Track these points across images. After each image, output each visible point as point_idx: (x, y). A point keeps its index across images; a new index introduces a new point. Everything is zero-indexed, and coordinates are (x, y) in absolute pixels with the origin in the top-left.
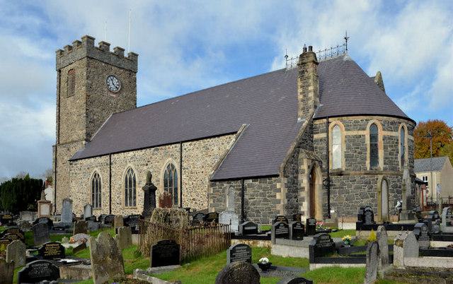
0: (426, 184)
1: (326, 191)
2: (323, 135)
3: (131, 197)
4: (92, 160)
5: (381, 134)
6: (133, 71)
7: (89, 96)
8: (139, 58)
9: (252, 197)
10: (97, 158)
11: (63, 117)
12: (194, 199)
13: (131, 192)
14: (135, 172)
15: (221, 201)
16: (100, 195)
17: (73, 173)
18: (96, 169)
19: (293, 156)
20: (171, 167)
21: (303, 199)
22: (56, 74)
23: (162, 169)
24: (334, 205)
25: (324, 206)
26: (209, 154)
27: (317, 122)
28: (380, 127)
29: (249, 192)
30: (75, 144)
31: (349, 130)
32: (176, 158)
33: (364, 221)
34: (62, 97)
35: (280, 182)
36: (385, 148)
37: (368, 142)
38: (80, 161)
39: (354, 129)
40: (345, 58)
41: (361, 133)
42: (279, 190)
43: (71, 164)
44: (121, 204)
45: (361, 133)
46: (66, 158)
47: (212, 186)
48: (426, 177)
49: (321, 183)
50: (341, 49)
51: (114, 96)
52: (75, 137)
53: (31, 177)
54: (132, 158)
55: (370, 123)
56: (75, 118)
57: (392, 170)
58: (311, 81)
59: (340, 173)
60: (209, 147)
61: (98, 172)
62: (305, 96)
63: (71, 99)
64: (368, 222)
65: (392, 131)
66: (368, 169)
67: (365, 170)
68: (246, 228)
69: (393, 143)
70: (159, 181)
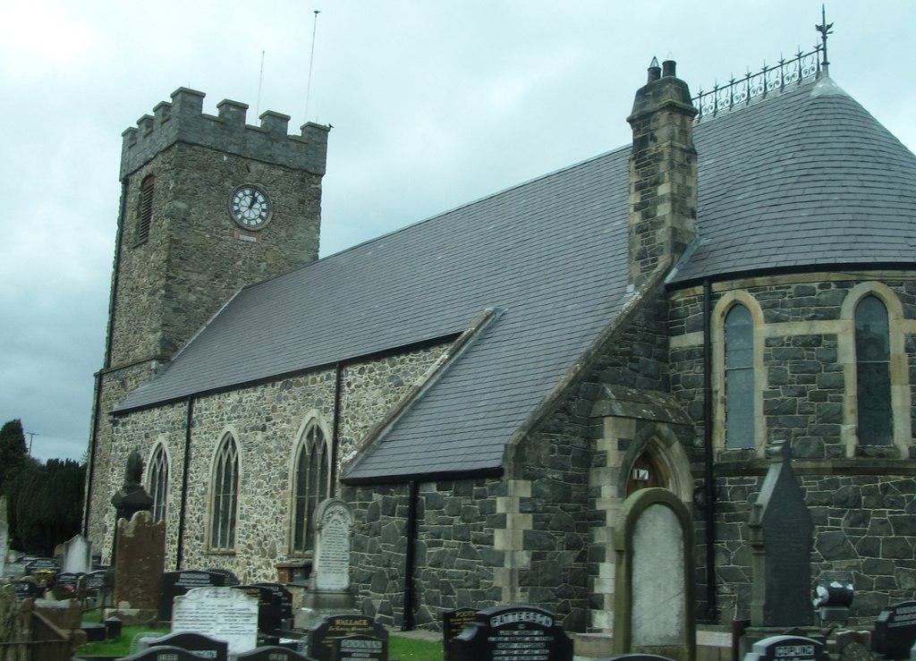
2: (695, 339)
4: (156, 412)
6: (313, 172)
7: (176, 242)
11: (124, 300)
18: (161, 439)
19: (565, 410)
20: (314, 433)
21: (599, 555)
23: (296, 441)
27: (679, 297)
28: (895, 306)
29: (429, 520)
30: (136, 370)
31: (777, 320)
34: (124, 248)
40: (820, 88)
41: (822, 327)
45: (822, 327)
50: (808, 63)
52: (139, 352)
55: (856, 293)
58: (663, 167)
60: (404, 379)
62: (646, 216)
63: (141, 251)
66: (850, 453)
70: (286, 476)
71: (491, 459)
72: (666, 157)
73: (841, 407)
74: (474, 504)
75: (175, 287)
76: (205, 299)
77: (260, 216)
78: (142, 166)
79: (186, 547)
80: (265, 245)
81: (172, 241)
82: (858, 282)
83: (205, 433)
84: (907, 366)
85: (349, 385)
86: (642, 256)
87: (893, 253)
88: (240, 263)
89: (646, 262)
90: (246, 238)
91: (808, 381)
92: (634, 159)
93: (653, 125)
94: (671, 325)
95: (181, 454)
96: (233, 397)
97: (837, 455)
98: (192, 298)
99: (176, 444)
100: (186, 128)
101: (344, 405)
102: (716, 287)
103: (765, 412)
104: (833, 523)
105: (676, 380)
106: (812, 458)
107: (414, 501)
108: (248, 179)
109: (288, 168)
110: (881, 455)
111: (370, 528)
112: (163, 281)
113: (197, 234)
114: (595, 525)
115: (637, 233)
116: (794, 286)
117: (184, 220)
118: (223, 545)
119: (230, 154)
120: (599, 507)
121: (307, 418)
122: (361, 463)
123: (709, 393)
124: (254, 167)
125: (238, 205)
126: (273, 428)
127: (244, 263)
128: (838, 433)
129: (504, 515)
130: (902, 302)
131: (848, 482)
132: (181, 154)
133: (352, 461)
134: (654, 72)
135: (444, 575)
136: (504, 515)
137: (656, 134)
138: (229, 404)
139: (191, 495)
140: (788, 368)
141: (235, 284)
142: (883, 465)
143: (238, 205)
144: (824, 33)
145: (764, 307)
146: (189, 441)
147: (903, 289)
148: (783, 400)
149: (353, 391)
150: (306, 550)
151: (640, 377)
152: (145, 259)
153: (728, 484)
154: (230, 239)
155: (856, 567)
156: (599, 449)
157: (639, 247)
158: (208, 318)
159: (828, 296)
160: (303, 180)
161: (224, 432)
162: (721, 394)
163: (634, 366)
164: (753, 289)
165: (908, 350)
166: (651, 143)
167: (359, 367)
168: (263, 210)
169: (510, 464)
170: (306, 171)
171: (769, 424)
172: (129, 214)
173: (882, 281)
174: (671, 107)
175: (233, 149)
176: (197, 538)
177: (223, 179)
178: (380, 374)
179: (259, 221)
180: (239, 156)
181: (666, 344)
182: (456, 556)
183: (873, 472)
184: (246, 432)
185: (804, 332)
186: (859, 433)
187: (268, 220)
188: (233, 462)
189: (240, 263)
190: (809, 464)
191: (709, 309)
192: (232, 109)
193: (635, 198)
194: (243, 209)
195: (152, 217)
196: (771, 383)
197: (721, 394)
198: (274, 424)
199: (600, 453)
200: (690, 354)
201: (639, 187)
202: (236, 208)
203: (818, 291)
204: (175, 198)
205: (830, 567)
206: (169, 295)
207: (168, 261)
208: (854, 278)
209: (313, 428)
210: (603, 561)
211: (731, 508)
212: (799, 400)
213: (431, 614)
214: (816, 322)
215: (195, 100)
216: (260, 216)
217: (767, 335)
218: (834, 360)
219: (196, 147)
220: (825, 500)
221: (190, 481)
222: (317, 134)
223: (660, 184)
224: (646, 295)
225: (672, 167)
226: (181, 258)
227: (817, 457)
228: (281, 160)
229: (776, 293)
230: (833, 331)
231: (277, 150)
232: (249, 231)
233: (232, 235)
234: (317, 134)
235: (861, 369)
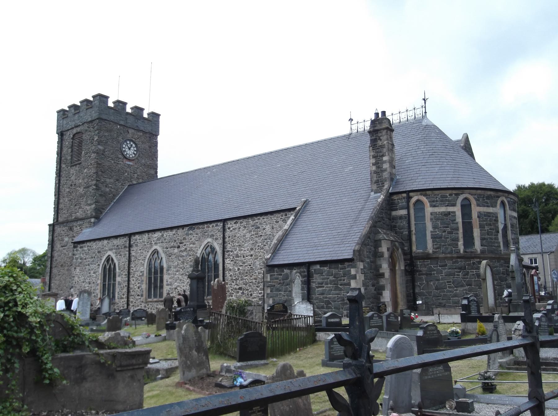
0: (537, 268)
1: (409, 278)
2: (404, 212)
3: (155, 287)
4: (105, 242)
5: (476, 210)
7: (100, 164)
8: (161, 119)
9: (320, 285)
10: (112, 240)
11: (65, 190)
12: (240, 289)
13: (156, 279)
14: (163, 255)
15: (280, 291)
16: (114, 285)
17: (77, 259)
18: (109, 253)
21: (383, 288)
22: (56, 138)
24: (421, 294)
25: (408, 296)
26: (260, 233)
27: (395, 197)
28: (474, 202)
31: (435, 206)
32: (216, 239)
33: (470, 312)
35: (355, 267)
36: (481, 227)
37: (459, 219)
38: (88, 244)
39: (441, 205)
40: (424, 123)
41: (450, 209)
42: (354, 277)
43: (75, 247)
44: (142, 296)
45: (450, 209)
46: (66, 239)
47: (268, 272)
48: (535, 260)
49: (403, 268)
51: (131, 163)
53: (546, 183)
54: (158, 239)
56: (81, 190)
57: (492, 252)
59: (427, 257)
61: (113, 256)
62: (378, 167)
64: (474, 314)
65: (488, 206)
66: (462, 251)
67: (458, 252)
68: (330, 320)
69: (491, 220)
71: (348, 255)
72: (386, 147)
73: (458, 236)
74: (340, 271)
75: (100, 185)
76: (113, 190)
77: (134, 153)
78: (73, 128)
79: (131, 300)
80: (136, 166)
81: (98, 164)
82: (462, 194)
83: (140, 250)
84: (478, 222)
85: (229, 228)
86: (377, 182)
87: (471, 184)
88: (126, 174)
89: (379, 184)
90: (129, 163)
91: (446, 227)
92: (371, 146)
93: (380, 135)
94: (392, 207)
95: (125, 260)
96: (158, 234)
97: (457, 252)
98: (108, 190)
99: (120, 255)
100: (102, 112)
101: (227, 236)
102: (411, 194)
103: (431, 238)
104: (457, 275)
105: (395, 226)
106: (449, 253)
107: (309, 271)
108: (128, 136)
109: (144, 132)
110: (472, 252)
111: (284, 283)
112: (94, 182)
113: (109, 161)
114: (379, 278)
115: (374, 173)
116: (440, 195)
117: (103, 154)
118: (155, 296)
119: (121, 125)
120: (381, 271)
121: (205, 242)
122: (272, 259)
123: (410, 232)
124: (131, 131)
125: (124, 148)
126: (185, 247)
127: (128, 174)
128: (457, 245)
129: (356, 275)
130: (476, 201)
131: (461, 261)
132: (99, 124)
133: (270, 258)
134: (377, 114)
135: (326, 298)
136: (356, 275)
137: (381, 138)
138: (155, 237)
139: (132, 277)
140: (439, 223)
141: (125, 183)
142: (473, 256)
143: (124, 148)
144: (425, 101)
145: (429, 202)
146: (130, 254)
147: (476, 196)
148: (438, 234)
149: (232, 231)
150: (207, 296)
151: (385, 226)
152: (80, 171)
153: (418, 263)
154: (122, 163)
155: (465, 290)
156: (380, 251)
157: (375, 179)
158: (114, 199)
159: (452, 198)
160: (150, 137)
161: (153, 249)
162: (414, 232)
163: (384, 222)
164: (425, 195)
165: (478, 217)
166: (379, 141)
167: (235, 221)
168: (135, 151)
169: (357, 257)
170: (152, 133)
171: (433, 242)
172: (65, 150)
173: (469, 194)
174: (387, 128)
175: (122, 123)
176: (138, 295)
177: (118, 136)
178: (247, 224)
179: (133, 155)
180: (125, 126)
181: (390, 214)
182: (332, 290)
183: (469, 258)
184: (167, 249)
185: (444, 211)
186: (465, 245)
187: (137, 155)
188: (112, 267)
189: (126, 174)
190: (449, 255)
191: (408, 202)
192: (121, 104)
193: (373, 161)
194: (127, 150)
195: (83, 152)
196: (433, 228)
197: (414, 232)
198: (185, 245)
199: (380, 252)
200: (401, 217)
201: (374, 157)
202: (124, 149)
203: (448, 196)
204: (99, 144)
205: (457, 290)
206: (98, 188)
207: (97, 173)
208: (461, 192)
209: (208, 246)
210: (384, 290)
211: (421, 271)
212: (443, 234)
213: (320, 312)
214: (448, 207)
215: (105, 99)
216: (134, 153)
217: (431, 211)
218: (455, 220)
219: (106, 121)
220: (454, 267)
221: (131, 271)
222: (155, 117)
223: (384, 156)
224: (385, 196)
225: (389, 150)
226: (102, 172)
227: (451, 253)
228: (142, 128)
229: (434, 197)
230: (454, 210)
231: (140, 124)
232: (129, 160)
233: (123, 162)
234: (155, 117)
235: (463, 223)
